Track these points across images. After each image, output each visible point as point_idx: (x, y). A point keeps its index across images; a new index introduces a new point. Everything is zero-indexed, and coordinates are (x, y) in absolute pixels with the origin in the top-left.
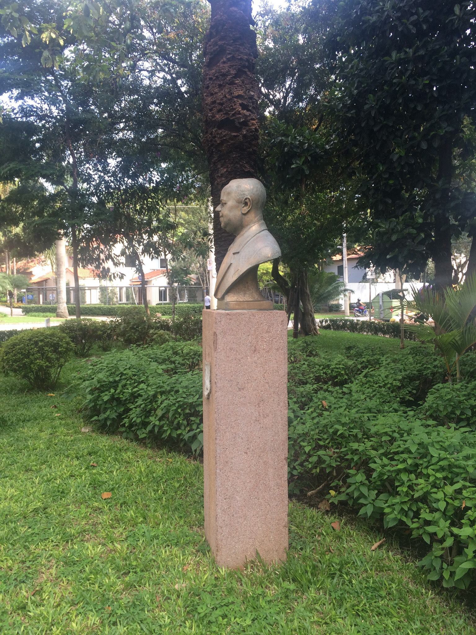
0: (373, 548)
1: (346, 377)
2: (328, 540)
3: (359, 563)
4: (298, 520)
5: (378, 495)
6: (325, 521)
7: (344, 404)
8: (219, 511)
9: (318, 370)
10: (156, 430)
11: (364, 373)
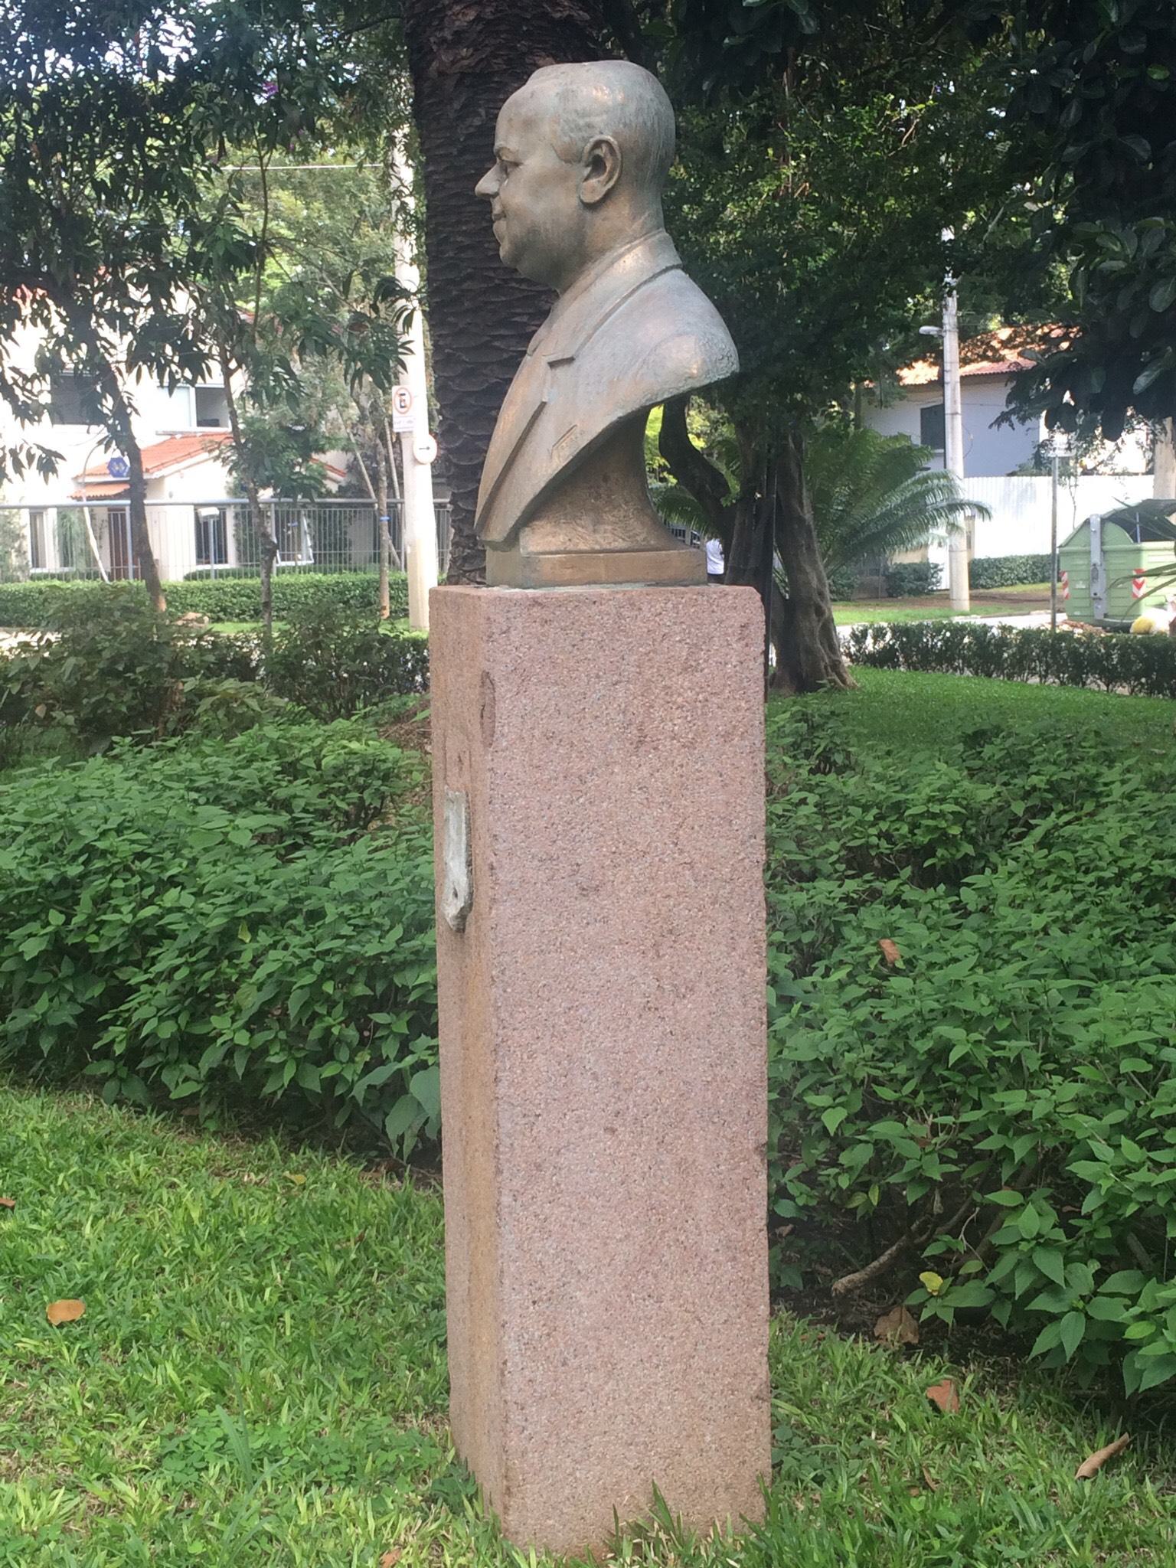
0: (1085, 1469)
1: (968, 849)
2: (917, 1449)
3: (1035, 1523)
4: (802, 1380)
5: (1100, 1277)
6: (900, 1382)
7: (966, 949)
8: (512, 1346)
9: (860, 823)
10: (240, 1066)
11: (1038, 834)
